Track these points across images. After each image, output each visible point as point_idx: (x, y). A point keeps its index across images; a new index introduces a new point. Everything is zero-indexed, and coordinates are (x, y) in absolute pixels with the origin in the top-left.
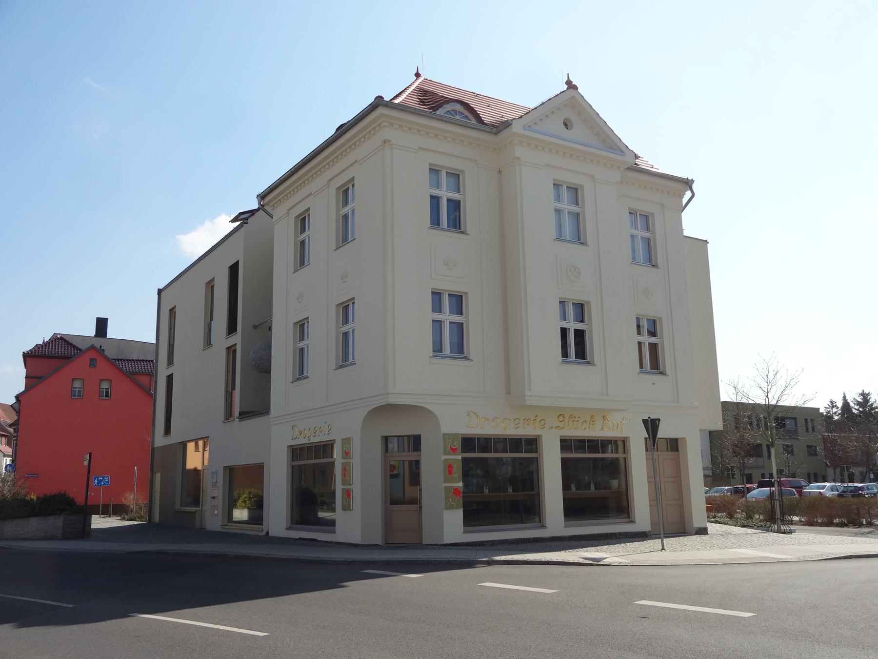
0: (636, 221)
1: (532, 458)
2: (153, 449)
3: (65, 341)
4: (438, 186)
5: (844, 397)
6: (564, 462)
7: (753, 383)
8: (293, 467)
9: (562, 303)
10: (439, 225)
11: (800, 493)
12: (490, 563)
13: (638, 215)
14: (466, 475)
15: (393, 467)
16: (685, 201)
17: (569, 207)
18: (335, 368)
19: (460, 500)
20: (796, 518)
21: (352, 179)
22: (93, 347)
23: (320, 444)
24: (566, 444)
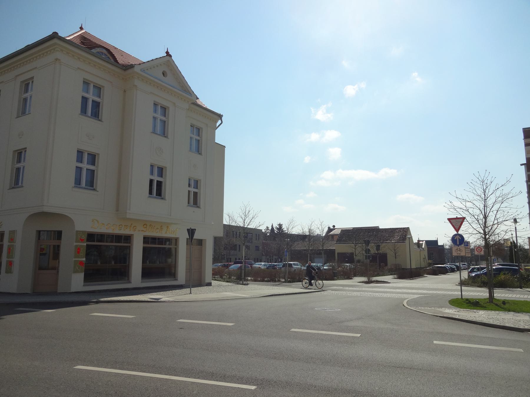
0: (193, 130)
1: (127, 246)
4: (87, 92)
5: (272, 225)
6: (144, 249)
7: (239, 215)
9: (152, 166)
10: (86, 113)
11: (251, 267)
12: (97, 302)
13: (195, 128)
14: (87, 255)
15: (42, 249)
16: (218, 124)
17: (160, 117)
18: (9, 188)
19: (83, 268)
20: (249, 278)
21: (32, 78)
24: (146, 240)
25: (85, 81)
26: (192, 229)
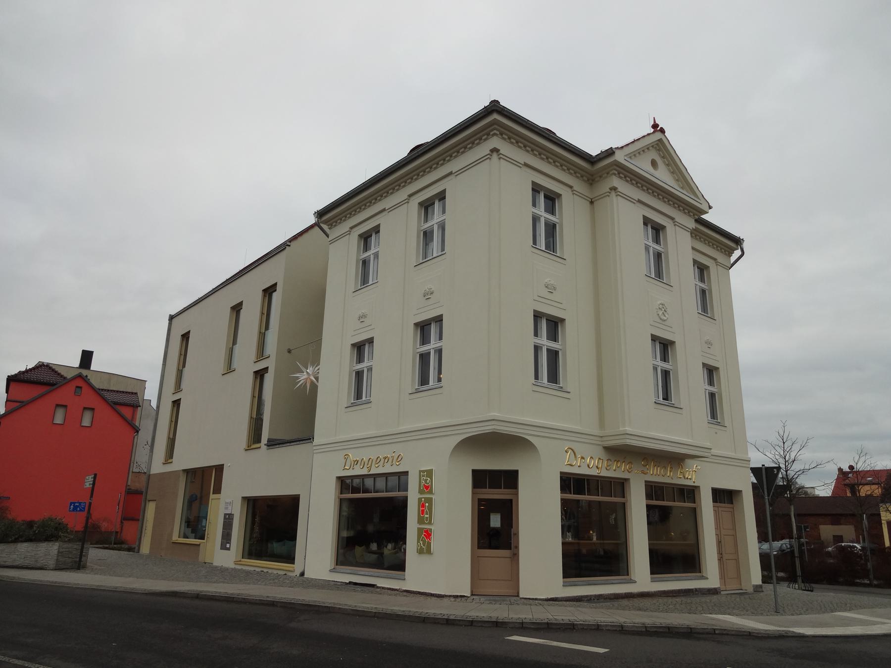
2: (149, 475)
3: (50, 368)
8: (341, 500)
25: (535, 188)
26: (767, 469)
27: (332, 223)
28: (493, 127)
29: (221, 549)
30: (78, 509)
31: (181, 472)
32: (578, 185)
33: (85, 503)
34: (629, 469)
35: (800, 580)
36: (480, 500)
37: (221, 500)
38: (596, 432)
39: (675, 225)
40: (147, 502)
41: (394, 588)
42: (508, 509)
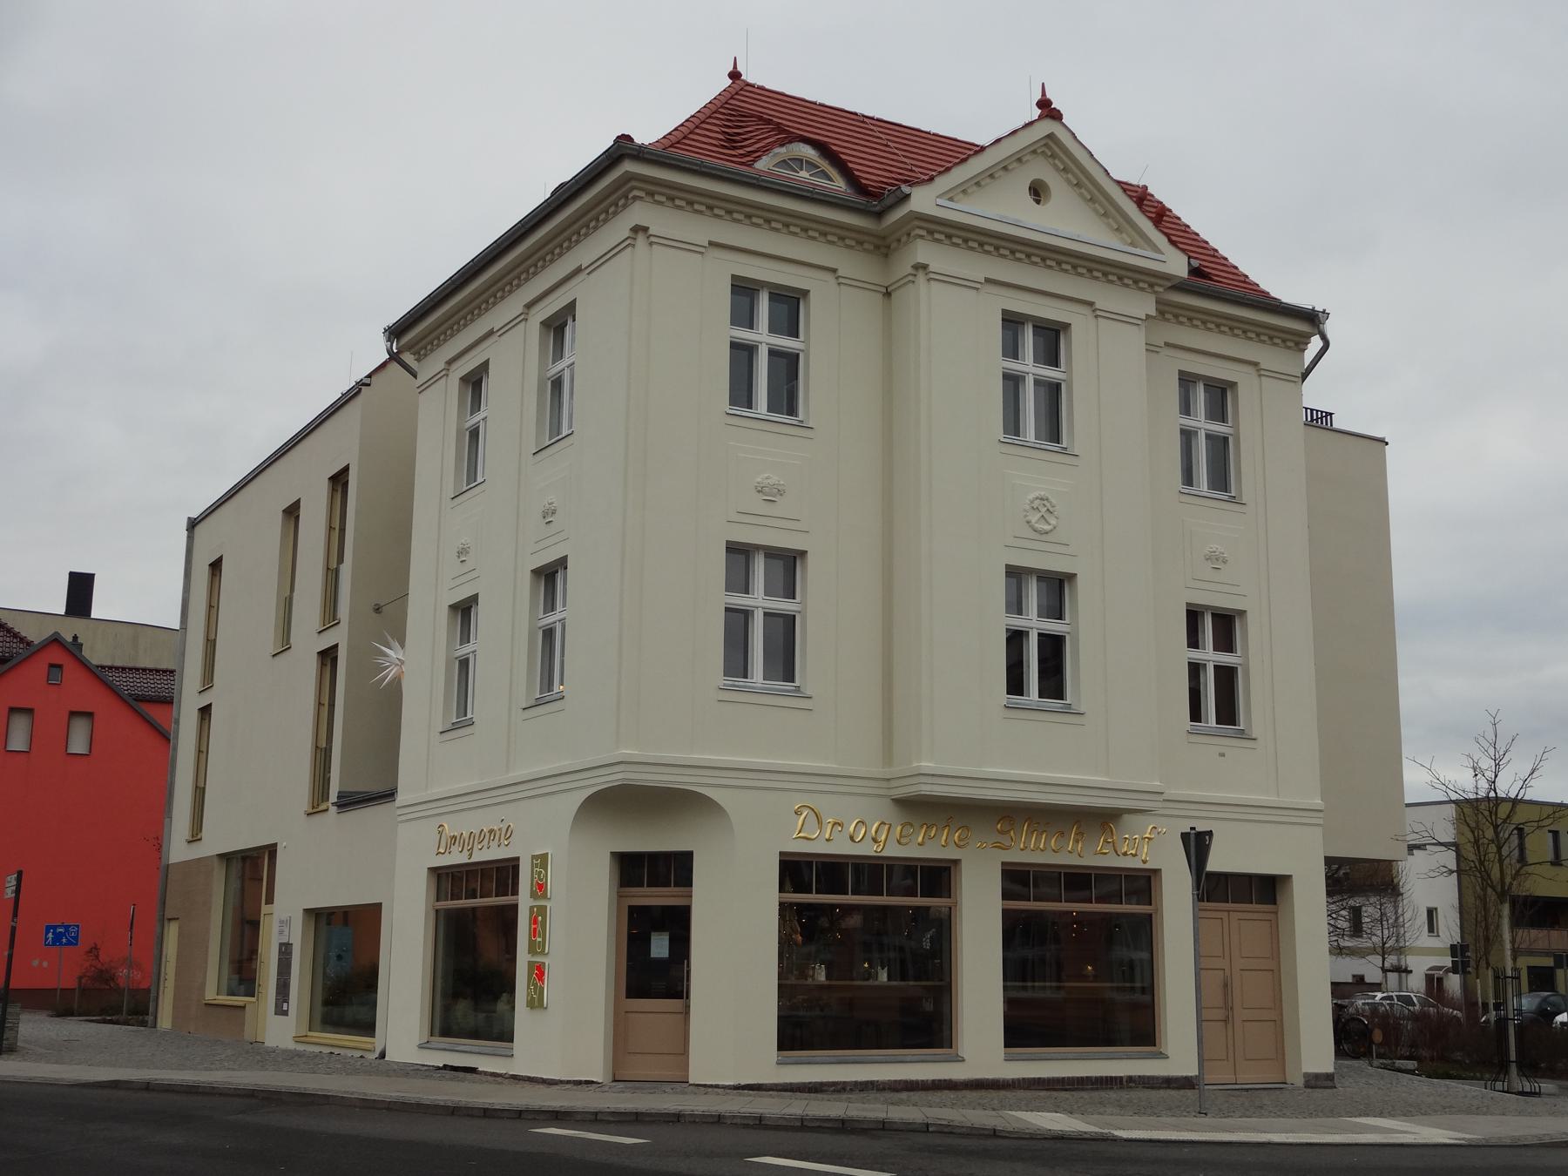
22: (56, 640)
23: (507, 864)
27: (422, 348)
28: (629, 185)
29: (276, 1014)
30: (64, 940)
31: (216, 860)
32: (850, 263)
33: (78, 926)
34: (959, 840)
35: (1514, 1069)
36: (633, 910)
37: (274, 915)
38: (877, 771)
39: (1096, 317)
40: (166, 922)
41: (498, 1071)
42: (677, 922)
